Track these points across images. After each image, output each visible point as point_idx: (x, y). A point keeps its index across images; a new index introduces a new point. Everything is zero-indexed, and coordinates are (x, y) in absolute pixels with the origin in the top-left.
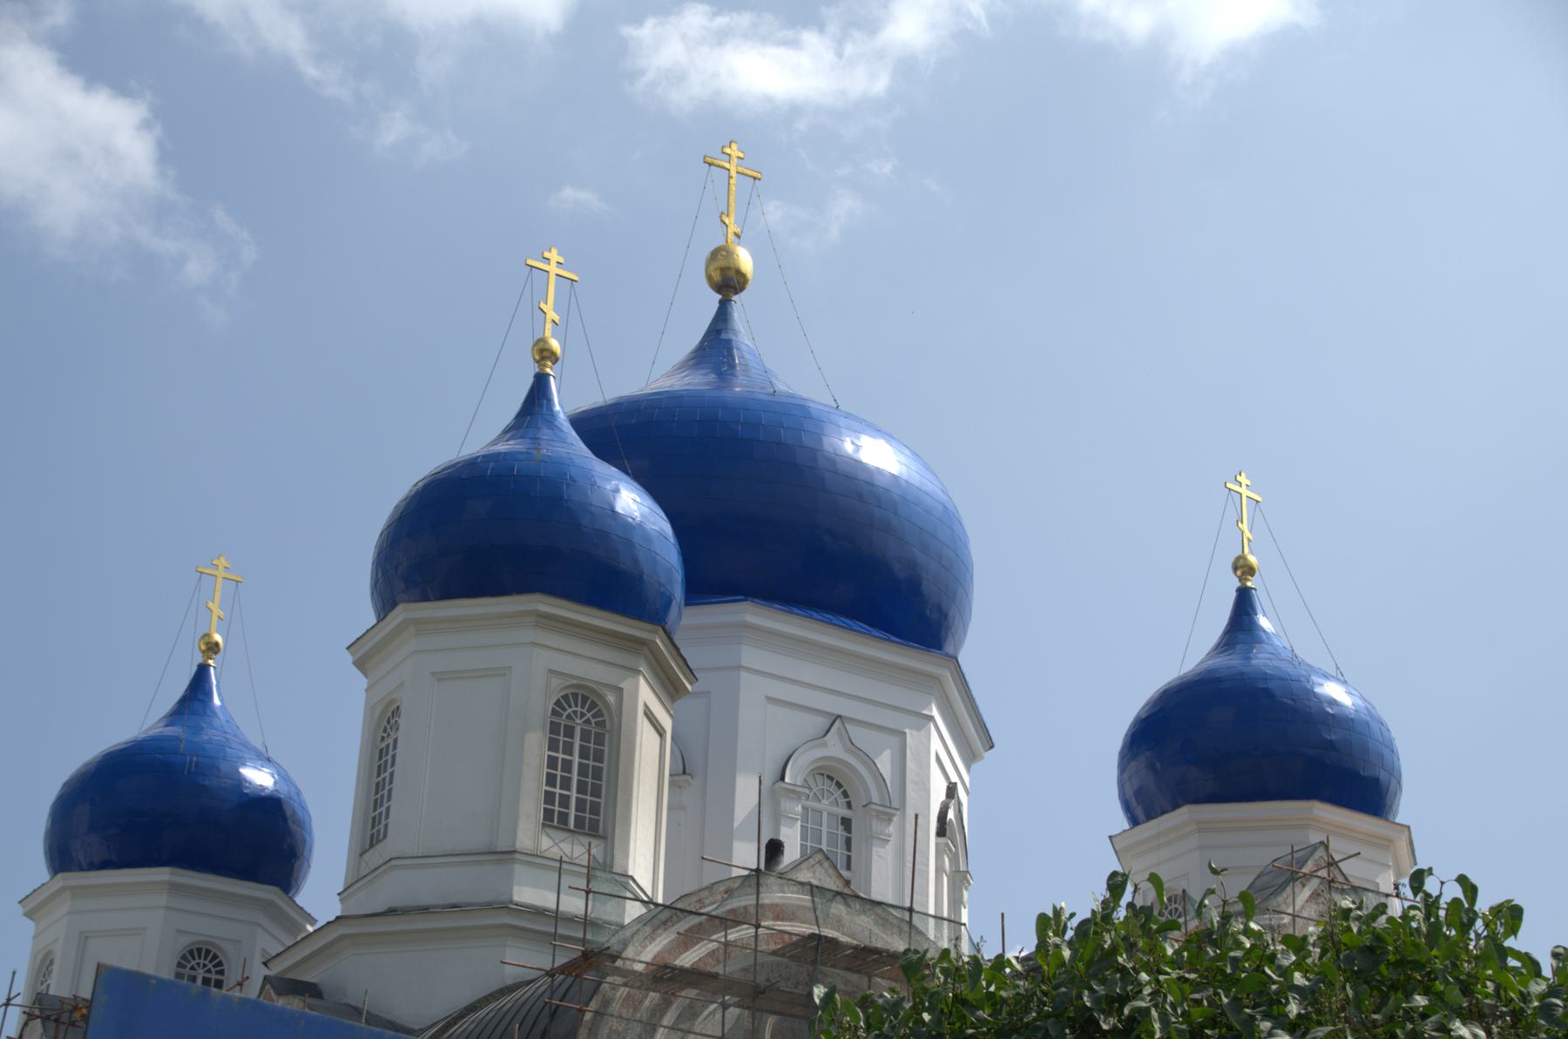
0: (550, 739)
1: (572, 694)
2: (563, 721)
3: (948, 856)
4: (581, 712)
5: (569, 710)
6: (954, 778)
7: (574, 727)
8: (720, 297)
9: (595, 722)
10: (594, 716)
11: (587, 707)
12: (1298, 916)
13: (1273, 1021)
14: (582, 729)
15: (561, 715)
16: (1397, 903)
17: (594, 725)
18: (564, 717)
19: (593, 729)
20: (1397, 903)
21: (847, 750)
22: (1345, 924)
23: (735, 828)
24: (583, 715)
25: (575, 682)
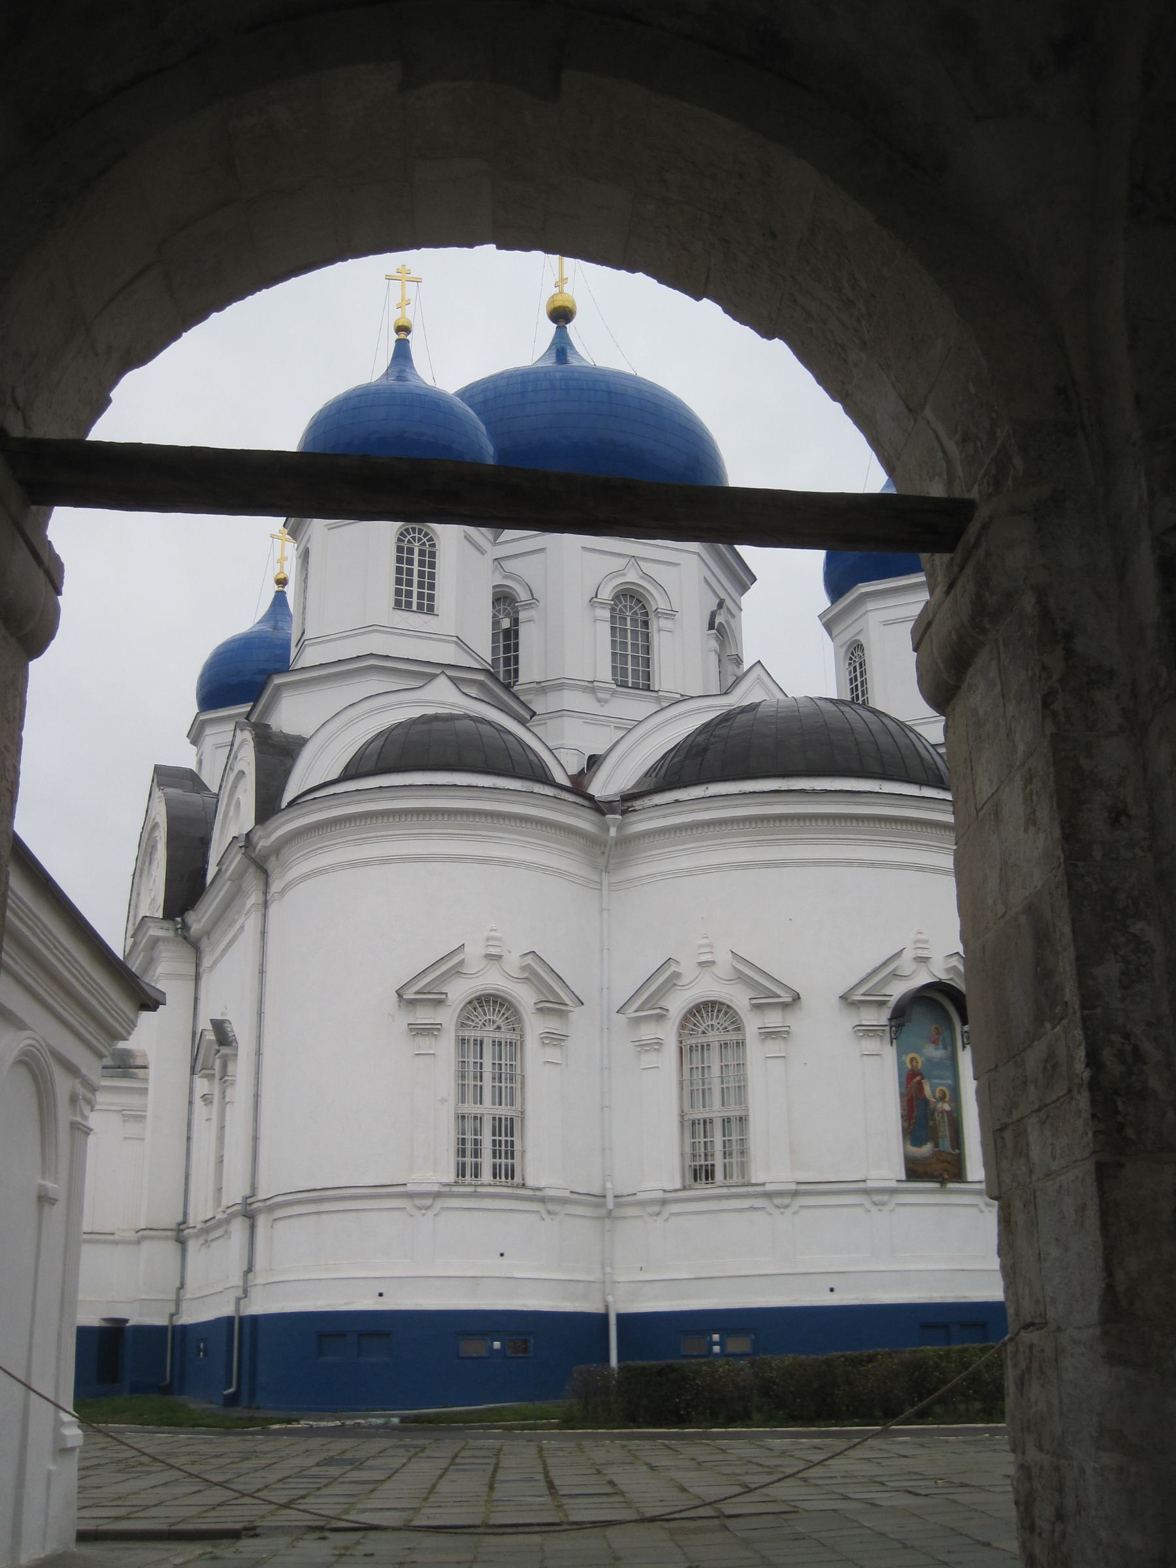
0: (612, 640)
1: (404, 530)
2: (405, 545)
3: (891, 1426)
4: (419, 538)
5: (409, 537)
6: (723, 595)
7: (413, 548)
8: (556, 325)
9: (641, 613)
10: (428, 541)
11: (406, 534)
12: (598, 883)
13: (941, 560)
14: (419, 549)
15: (404, 541)
16: (724, 550)
17: (428, 546)
18: (406, 543)
19: (427, 548)
20: (724, 550)
21: (641, 577)
22: (916, 1399)
23: (122, 959)
24: (631, 608)
25: (848, 643)
